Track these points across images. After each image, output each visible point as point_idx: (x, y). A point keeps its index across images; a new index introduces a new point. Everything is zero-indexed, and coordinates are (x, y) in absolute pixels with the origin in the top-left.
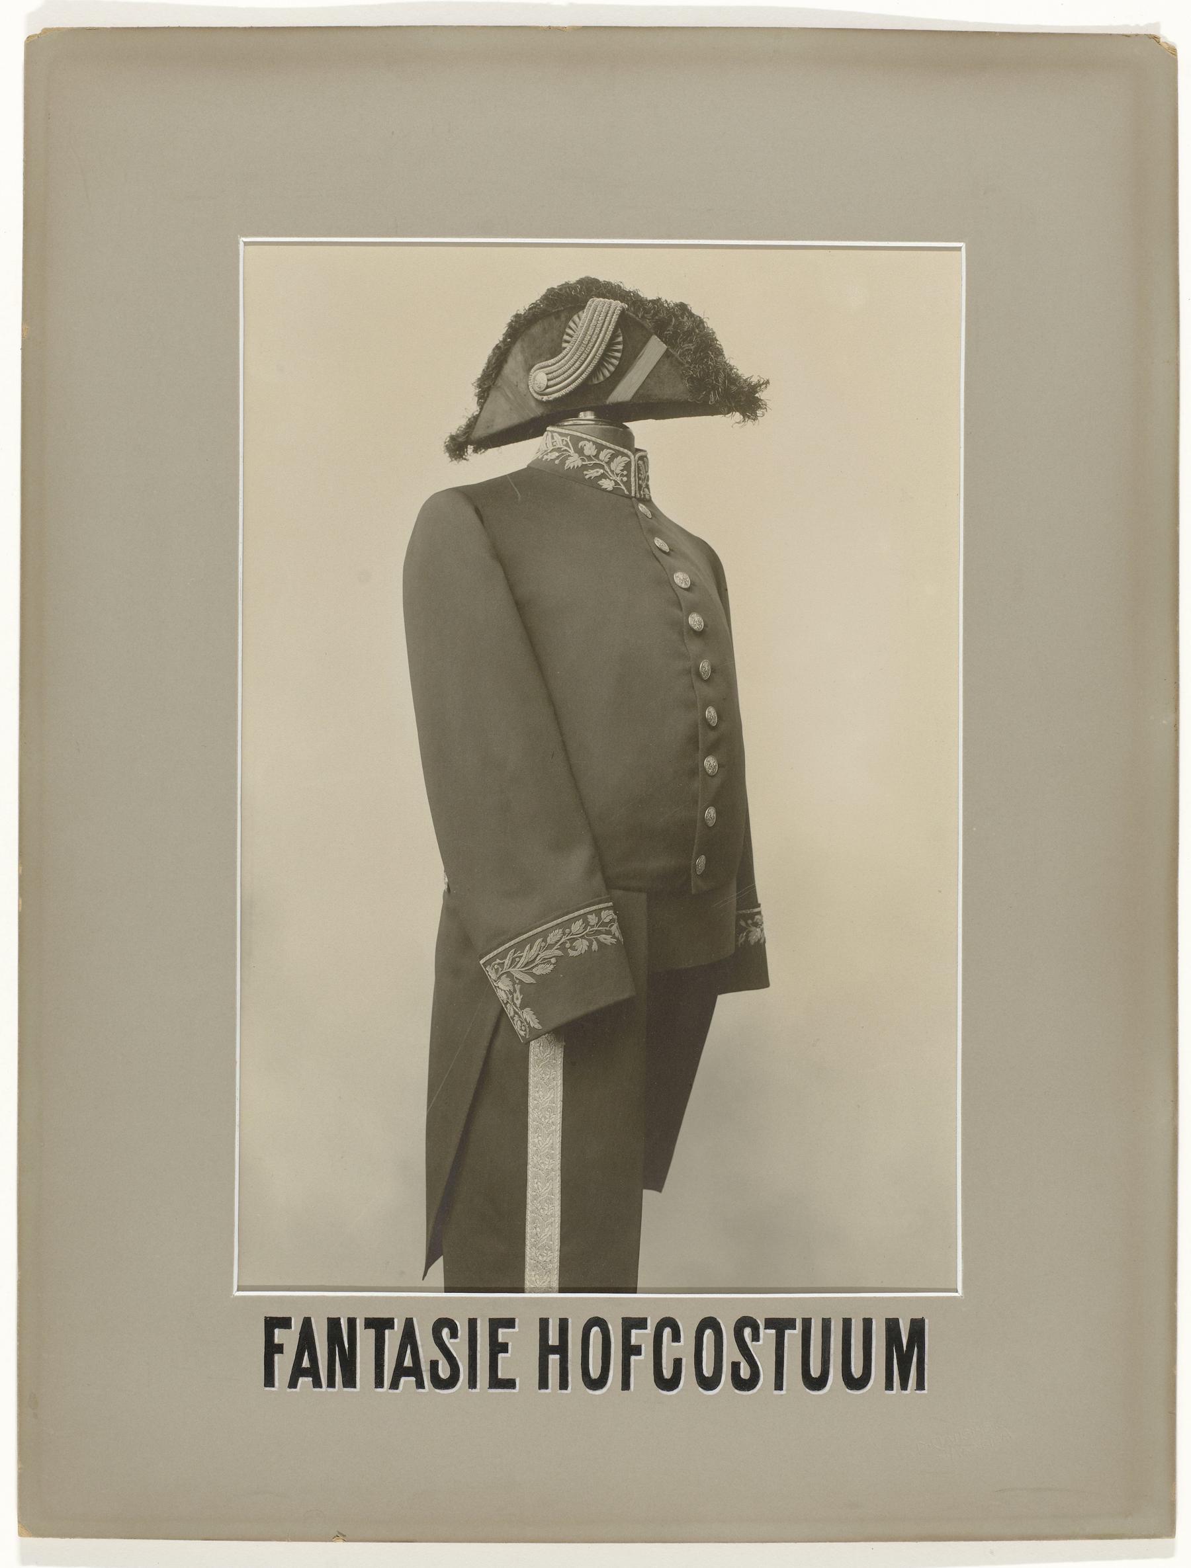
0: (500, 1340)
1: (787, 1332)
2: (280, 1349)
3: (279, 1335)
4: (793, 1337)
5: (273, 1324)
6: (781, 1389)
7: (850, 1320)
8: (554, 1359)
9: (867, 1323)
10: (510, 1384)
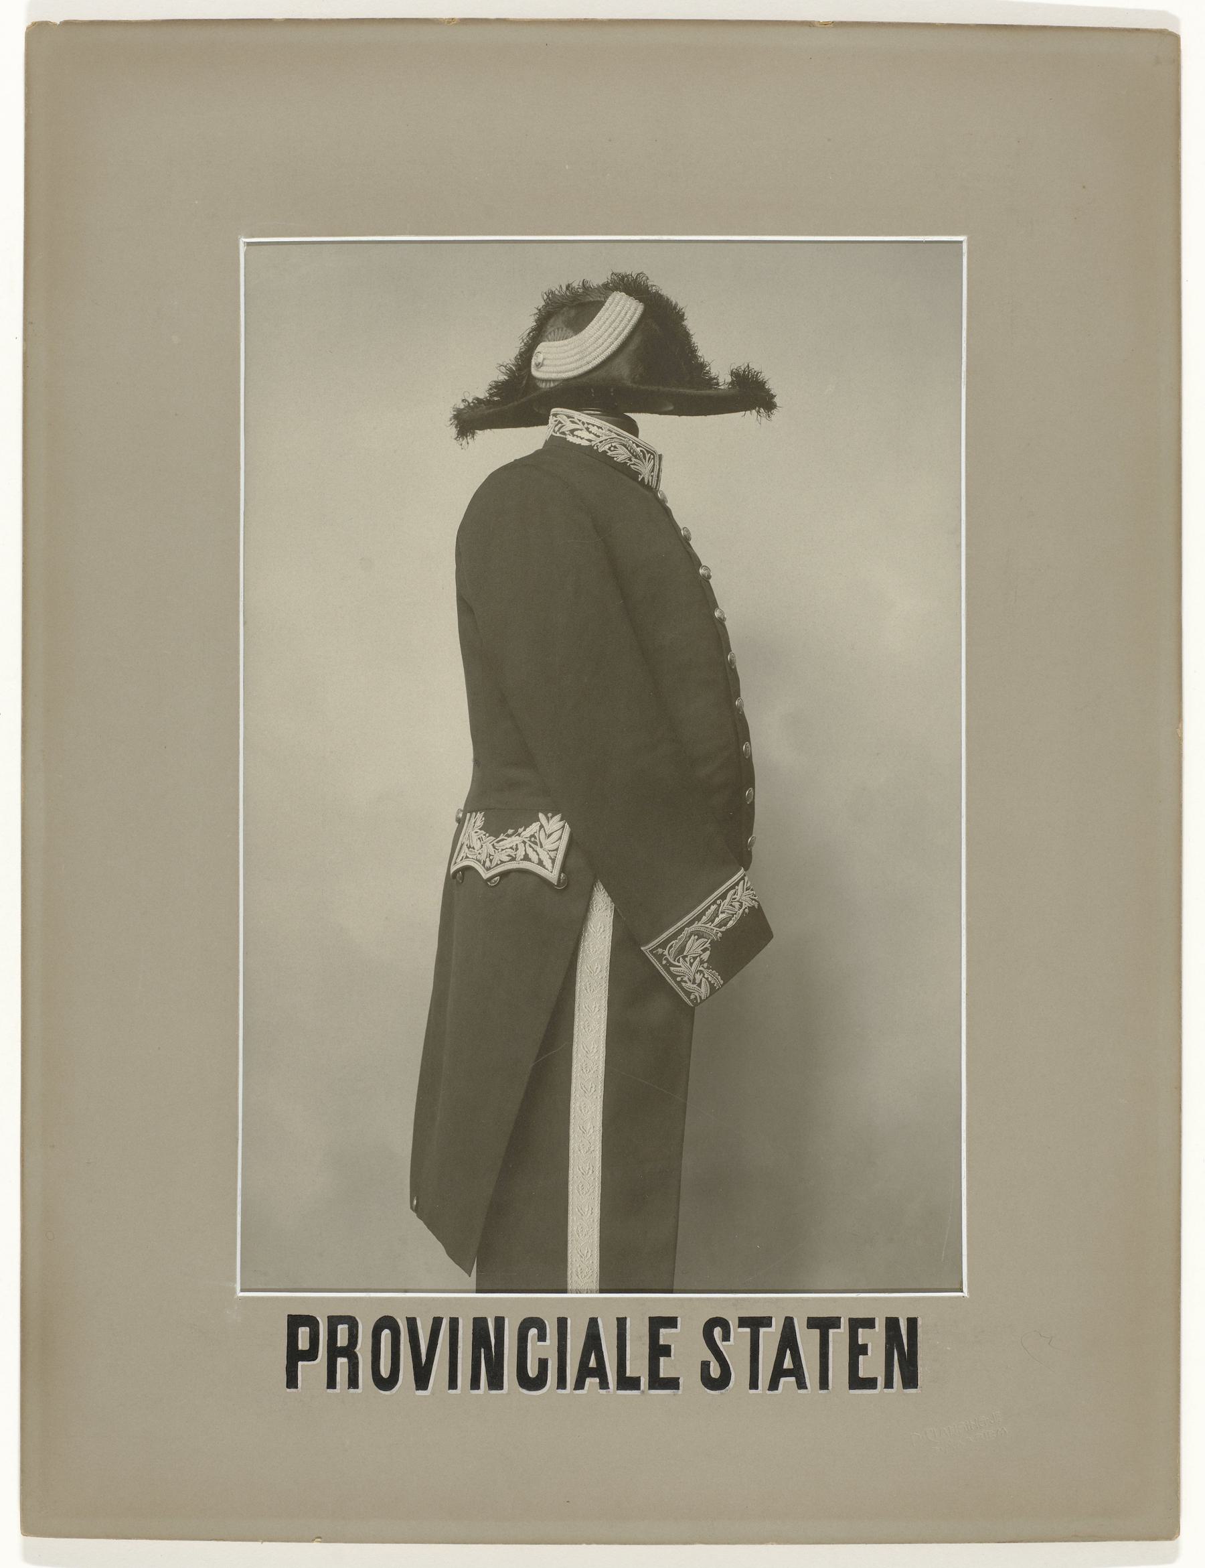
0: (662, 1342)
1: (831, 1331)
2: (863, 1350)
3: (863, 1335)
4: (839, 1338)
5: (295, 1322)
6: (757, 1388)
7: (503, 1319)
8: (342, 1362)
9: (454, 1323)
10: (672, 1383)
